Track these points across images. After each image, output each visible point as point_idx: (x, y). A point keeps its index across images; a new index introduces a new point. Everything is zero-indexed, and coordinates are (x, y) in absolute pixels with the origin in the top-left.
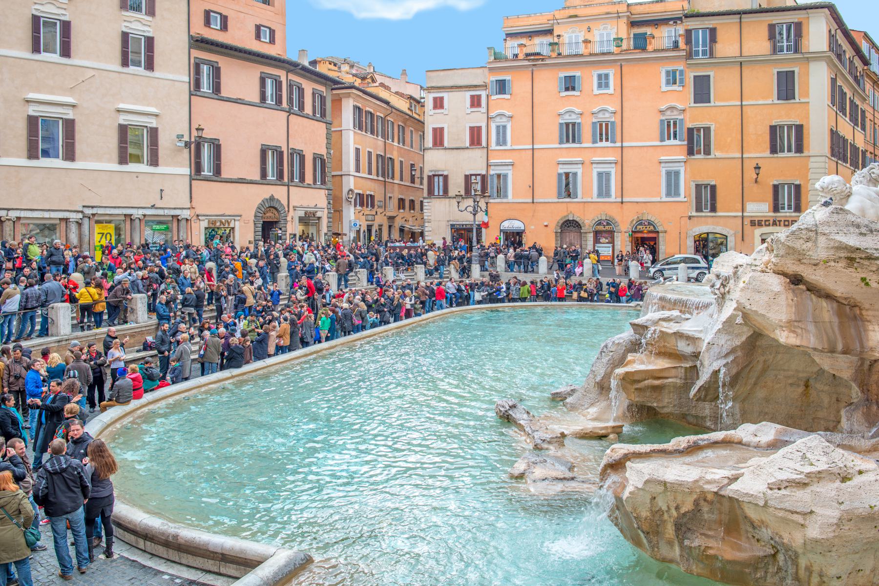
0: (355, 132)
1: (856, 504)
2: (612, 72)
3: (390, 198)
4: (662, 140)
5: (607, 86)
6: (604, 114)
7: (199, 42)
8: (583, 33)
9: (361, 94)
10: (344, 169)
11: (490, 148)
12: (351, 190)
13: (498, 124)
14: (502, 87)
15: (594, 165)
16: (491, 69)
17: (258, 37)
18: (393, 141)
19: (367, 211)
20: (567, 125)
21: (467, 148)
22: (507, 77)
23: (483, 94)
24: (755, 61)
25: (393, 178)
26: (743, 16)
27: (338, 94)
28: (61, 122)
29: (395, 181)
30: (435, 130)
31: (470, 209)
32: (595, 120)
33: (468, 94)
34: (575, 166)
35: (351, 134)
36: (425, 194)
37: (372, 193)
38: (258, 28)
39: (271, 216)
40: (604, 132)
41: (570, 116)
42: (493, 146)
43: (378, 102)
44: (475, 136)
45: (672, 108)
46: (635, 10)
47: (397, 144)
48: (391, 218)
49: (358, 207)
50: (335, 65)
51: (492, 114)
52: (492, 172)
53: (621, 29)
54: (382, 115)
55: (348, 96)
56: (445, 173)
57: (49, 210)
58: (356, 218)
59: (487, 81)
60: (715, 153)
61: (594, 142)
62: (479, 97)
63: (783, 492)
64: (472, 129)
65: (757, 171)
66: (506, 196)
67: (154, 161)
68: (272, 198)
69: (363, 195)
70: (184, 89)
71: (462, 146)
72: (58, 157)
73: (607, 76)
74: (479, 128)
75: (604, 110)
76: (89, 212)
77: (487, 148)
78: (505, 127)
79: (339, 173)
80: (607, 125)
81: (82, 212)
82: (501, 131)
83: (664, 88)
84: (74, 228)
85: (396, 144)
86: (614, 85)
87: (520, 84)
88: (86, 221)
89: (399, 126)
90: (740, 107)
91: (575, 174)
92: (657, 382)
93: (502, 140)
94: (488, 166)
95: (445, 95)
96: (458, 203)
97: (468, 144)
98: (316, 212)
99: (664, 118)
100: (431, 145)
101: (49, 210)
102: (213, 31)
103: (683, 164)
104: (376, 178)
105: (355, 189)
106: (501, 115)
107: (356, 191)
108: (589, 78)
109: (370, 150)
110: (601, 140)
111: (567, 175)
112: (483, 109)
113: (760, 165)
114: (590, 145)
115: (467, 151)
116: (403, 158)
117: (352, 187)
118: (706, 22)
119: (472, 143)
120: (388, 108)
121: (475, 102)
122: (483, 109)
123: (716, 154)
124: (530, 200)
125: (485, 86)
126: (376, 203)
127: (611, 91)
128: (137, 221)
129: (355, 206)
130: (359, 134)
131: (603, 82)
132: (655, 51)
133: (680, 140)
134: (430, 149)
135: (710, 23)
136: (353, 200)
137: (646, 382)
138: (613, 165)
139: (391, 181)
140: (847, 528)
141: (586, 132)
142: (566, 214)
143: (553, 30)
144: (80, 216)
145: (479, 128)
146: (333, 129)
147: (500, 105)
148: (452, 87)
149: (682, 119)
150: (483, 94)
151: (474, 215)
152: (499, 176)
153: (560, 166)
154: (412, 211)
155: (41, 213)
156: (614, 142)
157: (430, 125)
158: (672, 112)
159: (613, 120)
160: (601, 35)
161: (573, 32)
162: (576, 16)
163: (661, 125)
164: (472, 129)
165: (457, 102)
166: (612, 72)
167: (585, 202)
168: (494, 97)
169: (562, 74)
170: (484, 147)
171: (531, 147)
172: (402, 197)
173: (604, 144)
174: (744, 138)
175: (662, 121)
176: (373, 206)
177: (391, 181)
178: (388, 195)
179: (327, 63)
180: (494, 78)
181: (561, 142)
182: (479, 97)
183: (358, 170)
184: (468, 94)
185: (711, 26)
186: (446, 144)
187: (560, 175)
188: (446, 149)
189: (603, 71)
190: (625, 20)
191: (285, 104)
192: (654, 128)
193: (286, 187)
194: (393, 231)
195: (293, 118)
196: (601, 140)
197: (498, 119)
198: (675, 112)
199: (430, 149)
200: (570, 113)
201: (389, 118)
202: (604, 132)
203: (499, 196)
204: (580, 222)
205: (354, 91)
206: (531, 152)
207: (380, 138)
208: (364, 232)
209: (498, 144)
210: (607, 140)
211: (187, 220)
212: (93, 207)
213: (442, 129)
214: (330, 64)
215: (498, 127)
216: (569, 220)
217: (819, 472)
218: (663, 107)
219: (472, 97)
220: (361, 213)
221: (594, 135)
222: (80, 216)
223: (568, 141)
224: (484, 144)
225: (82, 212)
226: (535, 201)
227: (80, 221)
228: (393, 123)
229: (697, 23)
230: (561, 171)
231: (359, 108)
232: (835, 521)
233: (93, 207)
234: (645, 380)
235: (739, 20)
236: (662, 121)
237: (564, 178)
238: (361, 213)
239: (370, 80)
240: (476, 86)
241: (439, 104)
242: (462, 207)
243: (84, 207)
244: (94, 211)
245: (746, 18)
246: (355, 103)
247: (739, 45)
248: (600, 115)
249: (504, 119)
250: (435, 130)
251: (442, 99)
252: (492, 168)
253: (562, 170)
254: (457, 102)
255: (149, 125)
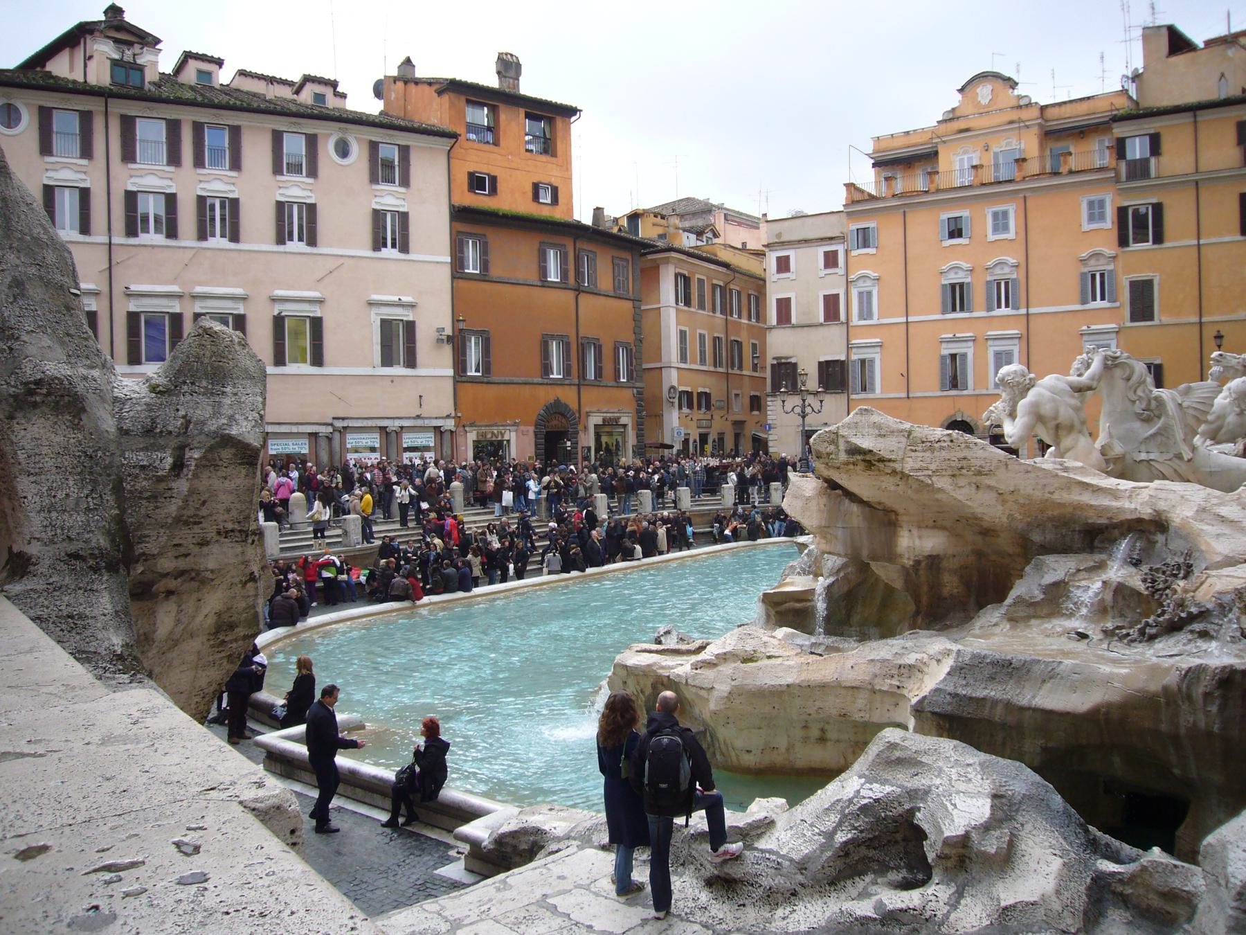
0: (677, 310)
1: (748, 681)
2: (1012, 209)
3: (737, 395)
4: (1084, 302)
5: (1005, 228)
6: (1002, 269)
7: (460, 214)
8: (978, 153)
9: (684, 257)
10: (664, 359)
11: (851, 324)
12: (673, 387)
13: (861, 290)
14: (864, 238)
15: (990, 343)
16: (850, 215)
17: (536, 197)
18: (740, 317)
19: (701, 414)
20: (953, 286)
21: (821, 325)
22: (871, 224)
23: (840, 249)
24: (1216, 179)
25: (740, 368)
26: (1198, 113)
27: (655, 260)
28: (308, 321)
29: (745, 372)
30: (779, 301)
31: (798, 410)
32: (989, 278)
33: (820, 251)
34: (964, 344)
35: (673, 313)
36: (769, 389)
37: (707, 390)
38: (536, 187)
39: (556, 423)
40: (1003, 293)
41: (956, 273)
42: (855, 321)
43: (712, 267)
44: (831, 303)
45: (1096, 255)
46: (1050, 113)
47: (746, 322)
48: (739, 424)
49: (685, 410)
50: (663, 217)
51: (852, 277)
52: (854, 357)
53: (1029, 144)
54: (721, 284)
55: (667, 261)
56: (793, 360)
57: (297, 424)
58: (680, 425)
59: (845, 230)
60: (1160, 316)
61: (990, 309)
62: (835, 253)
63: (698, 671)
64: (827, 299)
65: (1218, 341)
66: (873, 390)
67: (411, 362)
68: (557, 401)
69: (692, 393)
70: (446, 272)
71: (815, 321)
72: (306, 362)
73: (1005, 214)
74: (836, 296)
75: (1001, 264)
76: (339, 424)
77: (847, 323)
78: (869, 294)
79: (658, 365)
80: (1007, 284)
81: (331, 425)
82: (865, 298)
83: (1086, 227)
84: (323, 444)
85: (744, 321)
86: (1016, 227)
87: (888, 232)
88: (337, 436)
89: (749, 296)
90: (1196, 248)
91: (964, 356)
92: (798, 605)
93: (866, 313)
94: (849, 348)
95: (791, 253)
96: (783, 401)
97: (822, 319)
98: (619, 418)
99: (1086, 270)
100: (774, 322)
101: (297, 424)
102: (481, 197)
103: (1114, 335)
104: (712, 369)
105: (679, 384)
106: (865, 277)
107: (681, 388)
108: (981, 219)
109: (702, 332)
110: (1094, 299)
111: (953, 357)
112: (841, 270)
113: (1222, 333)
114: (984, 314)
115: (821, 329)
116: (756, 339)
117: (675, 383)
118: (1146, 126)
119: (827, 318)
120: (729, 272)
121: (831, 260)
122: (841, 270)
123: (1163, 319)
124: (904, 395)
125: (841, 239)
126: (713, 402)
127: (1011, 235)
128: (394, 435)
129: (680, 408)
130: (685, 311)
131: (1000, 222)
132: (1071, 172)
133: (1109, 302)
134: (774, 327)
135: (1152, 126)
136: (676, 401)
137: (787, 605)
138: (1016, 341)
139: (738, 372)
140: (738, 702)
141: (978, 295)
142: (952, 412)
143: (936, 153)
144: (330, 429)
145: (836, 296)
146: (643, 308)
147: (865, 263)
148: (799, 242)
149: (1112, 271)
150: (840, 249)
151: (803, 417)
152: (863, 362)
153: (944, 345)
154: (756, 413)
155: (288, 426)
156: (1016, 308)
157: (773, 296)
158: (1098, 260)
159: (1014, 276)
160: (962, 161)
161: (965, 153)
162: (967, 130)
163: (1082, 280)
164: (827, 299)
165: (807, 262)
166: (1012, 209)
167: (977, 395)
168: (854, 253)
169: (945, 216)
170: (842, 323)
171: (904, 320)
172: (757, 394)
173: (1004, 311)
174: (1203, 292)
175: (1083, 275)
176: (708, 407)
177: (738, 372)
178: (734, 392)
179: (652, 215)
180: (854, 226)
181: (943, 313)
182: (835, 253)
183: (683, 358)
184: (820, 251)
185: (1152, 131)
186: (794, 321)
187: (943, 357)
188: (794, 327)
189: (1000, 208)
190: (1035, 130)
191: (572, 281)
192: (1072, 283)
193: (575, 389)
194: (742, 441)
195: (584, 299)
196: (1094, 299)
197: (860, 283)
198: (1102, 261)
199: (774, 327)
200: (956, 270)
201: (732, 286)
202: (1003, 293)
203: (864, 389)
204: (972, 424)
205: (673, 254)
206: (904, 327)
207: (718, 314)
208: (695, 441)
209: (861, 317)
210: (1103, 298)
211: (452, 432)
212: (343, 419)
213: (788, 300)
214: (656, 216)
215: (860, 294)
216: (956, 421)
217: (725, 654)
218: (1084, 255)
219: (826, 254)
220: (689, 418)
221: (989, 298)
222: (330, 429)
223: (954, 310)
224: (843, 317)
225: (331, 425)
226: (911, 395)
227: (330, 436)
228: (739, 293)
229: (1133, 128)
230: (945, 352)
231: (684, 276)
232: (726, 695)
233: (343, 419)
234: (786, 602)
235: (1192, 120)
236: (1083, 275)
237: (948, 361)
238: (689, 418)
239: (710, 235)
240: (831, 239)
241: (783, 264)
242: (788, 407)
243: (334, 418)
244: (345, 424)
245: (1204, 116)
246: (678, 270)
247: (1194, 155)
248: (998, 271)
249: (869, 283)
250: (779, 301)
251: (787, 258)
252: (854, 350)
253: (946, 350)
254: (807, 262)
255: (405, 319)
